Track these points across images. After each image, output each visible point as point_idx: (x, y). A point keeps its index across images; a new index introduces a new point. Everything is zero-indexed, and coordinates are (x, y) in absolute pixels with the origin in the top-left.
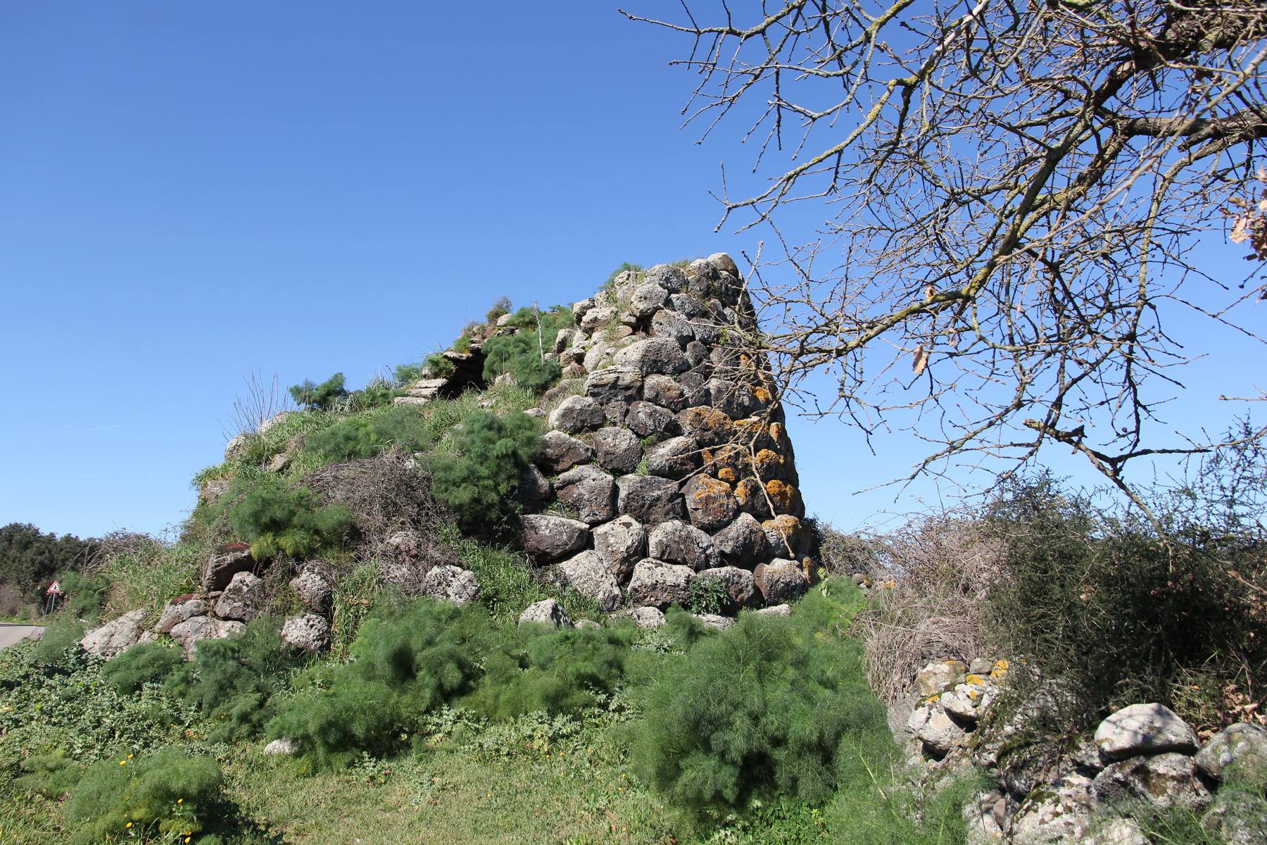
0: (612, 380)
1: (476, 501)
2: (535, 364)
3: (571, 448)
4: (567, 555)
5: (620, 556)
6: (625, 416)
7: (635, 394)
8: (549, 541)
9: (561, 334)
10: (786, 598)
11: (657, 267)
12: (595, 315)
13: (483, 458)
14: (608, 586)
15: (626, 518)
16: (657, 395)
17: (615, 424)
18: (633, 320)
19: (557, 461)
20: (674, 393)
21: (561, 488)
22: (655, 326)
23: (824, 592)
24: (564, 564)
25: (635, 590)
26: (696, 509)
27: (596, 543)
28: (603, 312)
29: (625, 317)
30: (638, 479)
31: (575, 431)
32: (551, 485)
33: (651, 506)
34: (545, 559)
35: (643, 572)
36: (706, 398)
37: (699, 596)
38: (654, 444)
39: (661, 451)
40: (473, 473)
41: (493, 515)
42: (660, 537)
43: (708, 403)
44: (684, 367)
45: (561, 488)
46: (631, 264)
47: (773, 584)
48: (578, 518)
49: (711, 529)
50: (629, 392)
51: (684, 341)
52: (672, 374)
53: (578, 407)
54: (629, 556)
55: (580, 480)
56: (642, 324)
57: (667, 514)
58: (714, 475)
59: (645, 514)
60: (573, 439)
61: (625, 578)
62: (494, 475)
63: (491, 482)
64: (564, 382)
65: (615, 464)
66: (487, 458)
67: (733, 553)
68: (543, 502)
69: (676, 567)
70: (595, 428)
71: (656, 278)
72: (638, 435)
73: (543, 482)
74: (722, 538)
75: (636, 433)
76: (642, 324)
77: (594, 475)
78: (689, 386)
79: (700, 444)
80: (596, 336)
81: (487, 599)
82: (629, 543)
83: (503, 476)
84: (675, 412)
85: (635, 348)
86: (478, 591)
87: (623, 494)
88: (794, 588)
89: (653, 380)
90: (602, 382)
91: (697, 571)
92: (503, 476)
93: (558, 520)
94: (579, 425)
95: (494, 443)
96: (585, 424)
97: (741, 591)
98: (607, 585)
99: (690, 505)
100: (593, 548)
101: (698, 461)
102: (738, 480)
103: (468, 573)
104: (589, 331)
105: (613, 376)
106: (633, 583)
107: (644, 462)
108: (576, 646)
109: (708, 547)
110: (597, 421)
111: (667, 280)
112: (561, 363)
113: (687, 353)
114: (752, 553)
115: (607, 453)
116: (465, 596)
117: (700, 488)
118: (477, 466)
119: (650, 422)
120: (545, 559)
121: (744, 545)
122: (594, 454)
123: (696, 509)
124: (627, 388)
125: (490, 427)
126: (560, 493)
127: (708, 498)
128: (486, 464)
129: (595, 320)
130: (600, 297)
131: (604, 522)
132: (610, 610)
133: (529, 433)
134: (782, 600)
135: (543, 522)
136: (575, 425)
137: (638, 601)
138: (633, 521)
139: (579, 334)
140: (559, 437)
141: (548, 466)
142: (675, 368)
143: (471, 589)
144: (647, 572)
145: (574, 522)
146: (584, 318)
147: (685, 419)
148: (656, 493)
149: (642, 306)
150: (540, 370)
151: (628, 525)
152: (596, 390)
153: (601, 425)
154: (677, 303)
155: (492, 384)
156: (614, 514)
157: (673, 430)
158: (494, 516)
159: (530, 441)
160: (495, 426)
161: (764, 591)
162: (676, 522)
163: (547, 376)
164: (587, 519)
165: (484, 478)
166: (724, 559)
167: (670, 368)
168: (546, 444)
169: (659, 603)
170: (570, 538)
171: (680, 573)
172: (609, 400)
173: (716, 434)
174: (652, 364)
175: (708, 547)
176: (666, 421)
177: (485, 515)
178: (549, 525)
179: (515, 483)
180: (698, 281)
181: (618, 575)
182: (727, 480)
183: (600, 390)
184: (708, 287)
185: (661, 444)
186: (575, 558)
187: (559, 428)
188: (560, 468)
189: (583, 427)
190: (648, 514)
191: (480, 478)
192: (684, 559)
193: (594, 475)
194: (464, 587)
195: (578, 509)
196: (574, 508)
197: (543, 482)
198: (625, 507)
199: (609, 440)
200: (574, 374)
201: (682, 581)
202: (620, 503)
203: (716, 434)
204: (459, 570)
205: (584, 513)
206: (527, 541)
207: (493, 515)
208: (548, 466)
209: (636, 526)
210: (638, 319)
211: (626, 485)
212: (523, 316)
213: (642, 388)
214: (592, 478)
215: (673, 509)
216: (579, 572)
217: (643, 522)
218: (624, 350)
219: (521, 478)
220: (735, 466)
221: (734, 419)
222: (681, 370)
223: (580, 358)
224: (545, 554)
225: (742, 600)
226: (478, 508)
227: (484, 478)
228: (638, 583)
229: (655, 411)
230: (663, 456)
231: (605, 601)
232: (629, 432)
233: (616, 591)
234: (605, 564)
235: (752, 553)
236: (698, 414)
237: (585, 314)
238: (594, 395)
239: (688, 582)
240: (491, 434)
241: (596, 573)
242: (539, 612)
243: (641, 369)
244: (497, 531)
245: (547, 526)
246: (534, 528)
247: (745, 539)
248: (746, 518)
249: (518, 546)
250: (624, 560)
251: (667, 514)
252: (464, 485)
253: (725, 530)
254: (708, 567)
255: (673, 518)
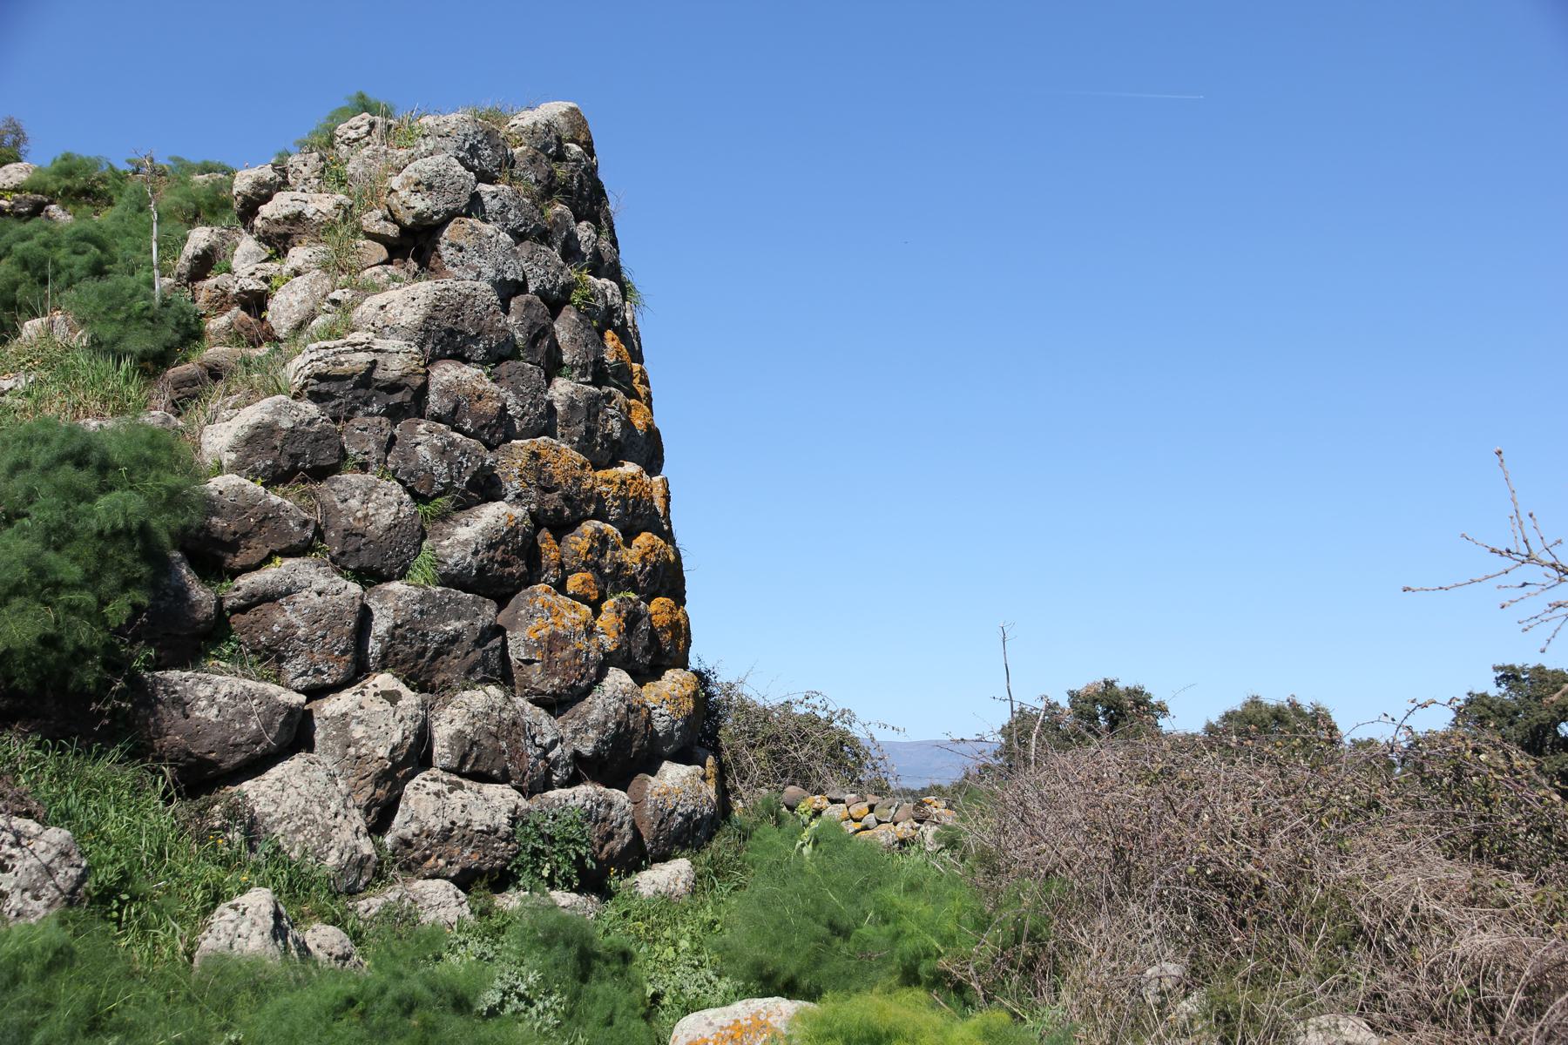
0: (362, 368)
1: (48, 641)
2: (140, 304)
3: (270, 517)
4: (256, 766)
5: (374, 767)
6: (388, 451)
7: (408, 401)
8: (218, 734)
9: (200, 238)
10: (684, 846)
11: (453, 118)
12: (298, 207)
13: (59, 537)
14: (349, 837)
15: (385, 680)
16: (456, 409)
17: (364, 467)
18: (392, 230)
19: (234, 547)
20: (490, 407)
21: (242, 610)
22: (446, 253)
23: (807, 850)
24: (247, 786)
25: (406, 843)
26: (529, 662)
27: (319, 736)
28: (321, 204)
29: (373, 221)
30: (416, 593)
31: (275, 478)
32: (220, 601)
33: (438, 653)
34: (202, 777)
35: (425, 803)
36: (546, 423)
37: (536, 853)
38: (444, 517)
39: (463, 533)
40: (40, 572)
41: (90, 675)
42: (458, 725)
43: (549, 431)
44: (507, 350)
45: (242, 610)
46: (372, 96)
47: (665, 817)
48: (277, 678)
49: (556, 704)
50: (397, 398)
51: (509, 290)
52: (483, 363)
53: (286, 423)
54: (397, 766)
55: (288, 592)
56: (415, 244)
57: (471, 671)
58: (560, 587)
59: (423, 670)
60: (275, 499)
61: (381, 816)
62: (92, 579)
63: (88, 598)
64: (213, 352)
65: (365, 559)
66: (72, 537)
67: (597, 753)
68: (197, 641)
69: (490, 789)
70: (321, 473)
71: (449, 144)
72: (417, 498)
73: (202, 595)
74: (576, 723)
75: (410, 490)
76: (415, 244)
77: (321, 582)
78: (517, 392)
79: (538, 520)
80: (298, 255)
81: (105, 896)
82: (397, 737)
83: (111, 580)
84: (491, 447)
85: (404, 300)
86: (82, 879)
87: (380, 626)
88: (698, 825)
89: (446, 374)
90: (339, 370)
91: (528, 792)
92: (111, 580)
93: (239, 684)
94: (285, 464)
95: (90, 499)
96: (296, 462)
97: (610, 836)
98: (347, 835)
99: (516, 653)
100: (310, 749)
101: (531, 554)
102: (603, 598)
103: (58, 835)
104: (278, 242)
105: (363, 358)
106: (401, 825)
107: (426, 554)
108: (375, 1021)
109: (553, 744)
110: (326, 457)
111: (473, 150)
112: (201, 305)
113: (511, 320)
114: (625, 757)
115: (349, 533)
116: (49, 892)
117: (540, 616)
118: (50, 556)
119: (441, 469)
120: (202, 777)
121: (616, 737)
122: (319, 533)
123: (529, 662)
124: (394, 387)
125: (79, 460)
126: (238, 621)
127: (554, 636)
128: (71, 551)
129: (297, 218)
130: (304, 164)
131: (337, 688)
132: (352, 892)
133: (172, 480)
134: (676, 850)
135: (204, 691)
136: (276, 466)
137: (411, 868)
138: (402, 688)
139: (247, 244)
140: (241, 491)
141: (212, 557)
142: (489, 351)
143: (66, 875)
144: (431, 804)
145: (272, 689)
146: (266, 210)
147: (512, 461)
148: (452, 626)
149: (420, 204)
150: (150, 318)
151: (392, 697)
152: (324, 387)
153: (335, 469)
154: (491, 205)
155: (17, 334)
156: (359, 671)
157: (486, 488)
158: (90, 679)
159: (174, 500)
160: (94, 456)
161: (647, 834)
162: (492, 689)
163: (169, 334)
164: (299, 682)
165: (74, 586)
166: (583, 769)
167: (480, 349)
168: (211, 506)
169: (455, 870)
170: (268, 726)
171: (493, 804)
172: (352, 411)
173: (567, 499)
174: (445, 338)
175: (553, 744)
176: (472, 466)
177: (67, 674)
178: (216, 696)
179: (142, 598)
180: (533, 160)
181: (368, 810)
182: (584, 599)
183: (333, 387)
184: (551, 175)
185: (461, 517)
186: (276, 772)
187: (236, 468)
188: (239, 561)
189: (294, 471)
190: (430, 671)
191: (58, 586)
192: (505, 771)
193: (321, 582)
194: (48, 871)
195: (281, 659)
196: (272, 656)
197: (202, 595)
198: (384, 655)
199: (354, 503)
200: (236, 336)
201: (503, 820)
202: (374, 647)
203: (567, 499)
204: (33, 827)
205: (292, 668)
206: (161, 734)
207: (90, 675)
208: (212, 557)
209: (410, 698)
210: (404, 230)
211: (392, 602)
212: (69, 173)
213: (424, 389)
214: (315, 587)
215: (484, 661)
216: (286, 807)
217: (421, 688)
218: (379, 299)
219: (153, 586)
220: (597, 568)
221: (596, 467)
222: (499, 356)
223: (255, 303)
224: (202, 763)
225: (610, 855)
226: (52, 657)
227: (74, 586)
228: (414, 827)
229: (452, 443)
230: (466, 543)
231: (342, 871)
232: (397, 489)
233: (366, 847)
234: (342, 785)
235: (625, 757)
236: (535, 456)
237: (267, 199)
238: (316, 397)
239: (513, 821)
240: (84, 478)
241: (326, 808)
242: (242, 925)
243: (421, 346)
244: (101, 713)
245: (212, 700)
246: (182, 704)
247: (619, 724)
248: (618, 679)
249: (140, 752)
250: (384, 777)
251: (471, 671)
252: (17, 602)
253: (582, 707)
254: (548, 786)
255: (486, 681)
